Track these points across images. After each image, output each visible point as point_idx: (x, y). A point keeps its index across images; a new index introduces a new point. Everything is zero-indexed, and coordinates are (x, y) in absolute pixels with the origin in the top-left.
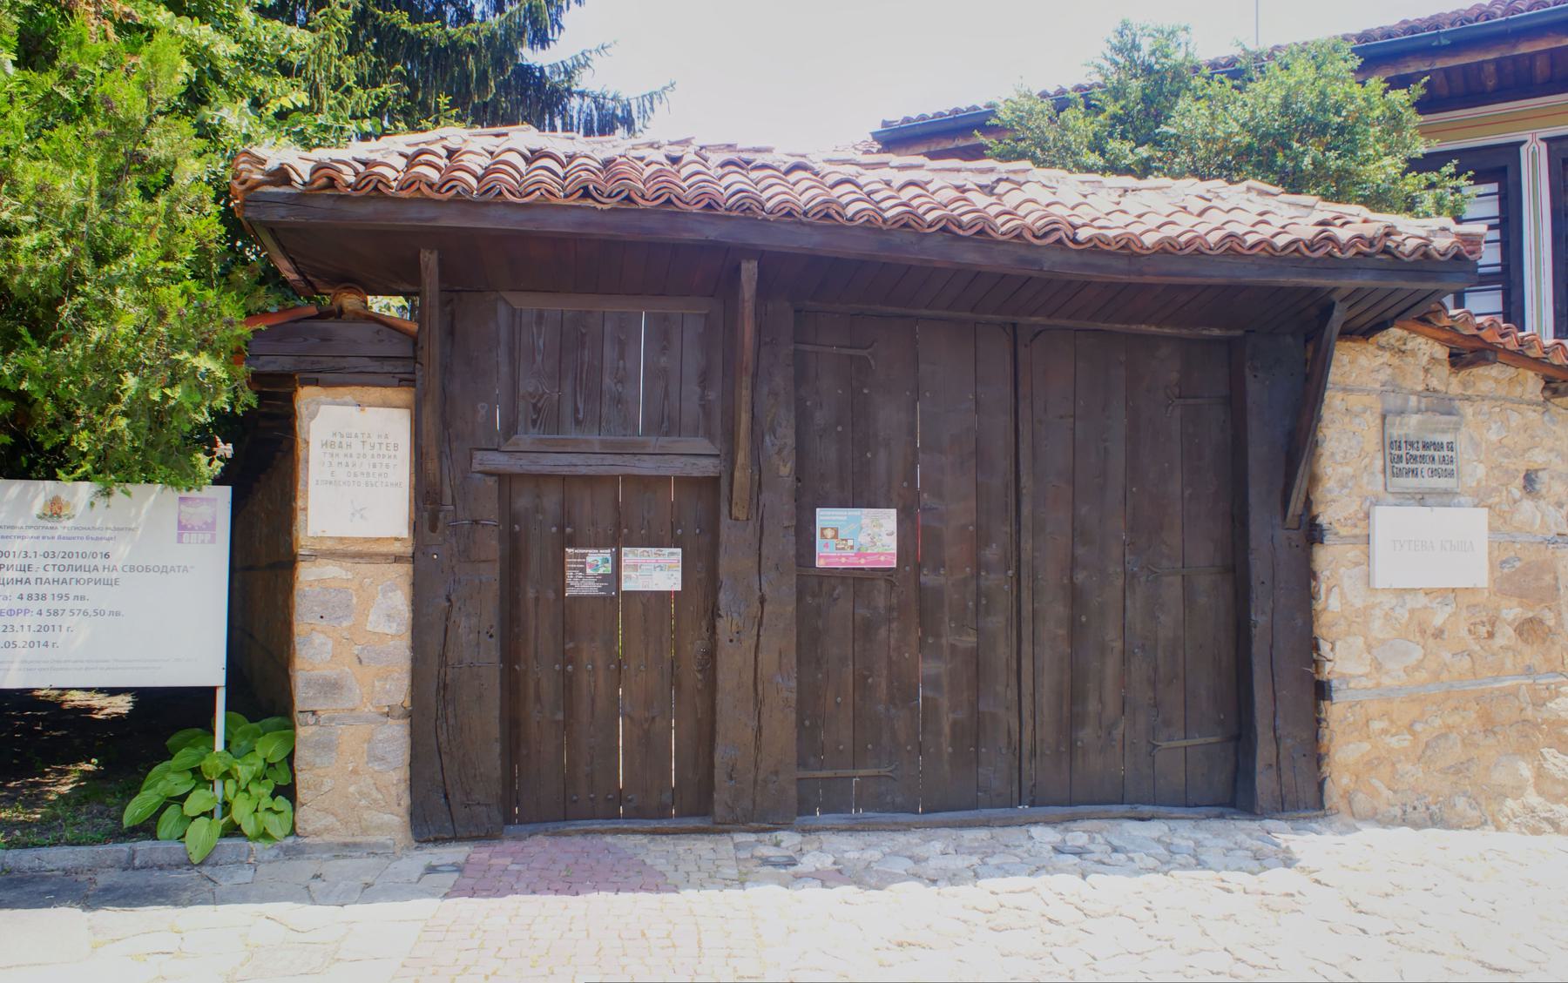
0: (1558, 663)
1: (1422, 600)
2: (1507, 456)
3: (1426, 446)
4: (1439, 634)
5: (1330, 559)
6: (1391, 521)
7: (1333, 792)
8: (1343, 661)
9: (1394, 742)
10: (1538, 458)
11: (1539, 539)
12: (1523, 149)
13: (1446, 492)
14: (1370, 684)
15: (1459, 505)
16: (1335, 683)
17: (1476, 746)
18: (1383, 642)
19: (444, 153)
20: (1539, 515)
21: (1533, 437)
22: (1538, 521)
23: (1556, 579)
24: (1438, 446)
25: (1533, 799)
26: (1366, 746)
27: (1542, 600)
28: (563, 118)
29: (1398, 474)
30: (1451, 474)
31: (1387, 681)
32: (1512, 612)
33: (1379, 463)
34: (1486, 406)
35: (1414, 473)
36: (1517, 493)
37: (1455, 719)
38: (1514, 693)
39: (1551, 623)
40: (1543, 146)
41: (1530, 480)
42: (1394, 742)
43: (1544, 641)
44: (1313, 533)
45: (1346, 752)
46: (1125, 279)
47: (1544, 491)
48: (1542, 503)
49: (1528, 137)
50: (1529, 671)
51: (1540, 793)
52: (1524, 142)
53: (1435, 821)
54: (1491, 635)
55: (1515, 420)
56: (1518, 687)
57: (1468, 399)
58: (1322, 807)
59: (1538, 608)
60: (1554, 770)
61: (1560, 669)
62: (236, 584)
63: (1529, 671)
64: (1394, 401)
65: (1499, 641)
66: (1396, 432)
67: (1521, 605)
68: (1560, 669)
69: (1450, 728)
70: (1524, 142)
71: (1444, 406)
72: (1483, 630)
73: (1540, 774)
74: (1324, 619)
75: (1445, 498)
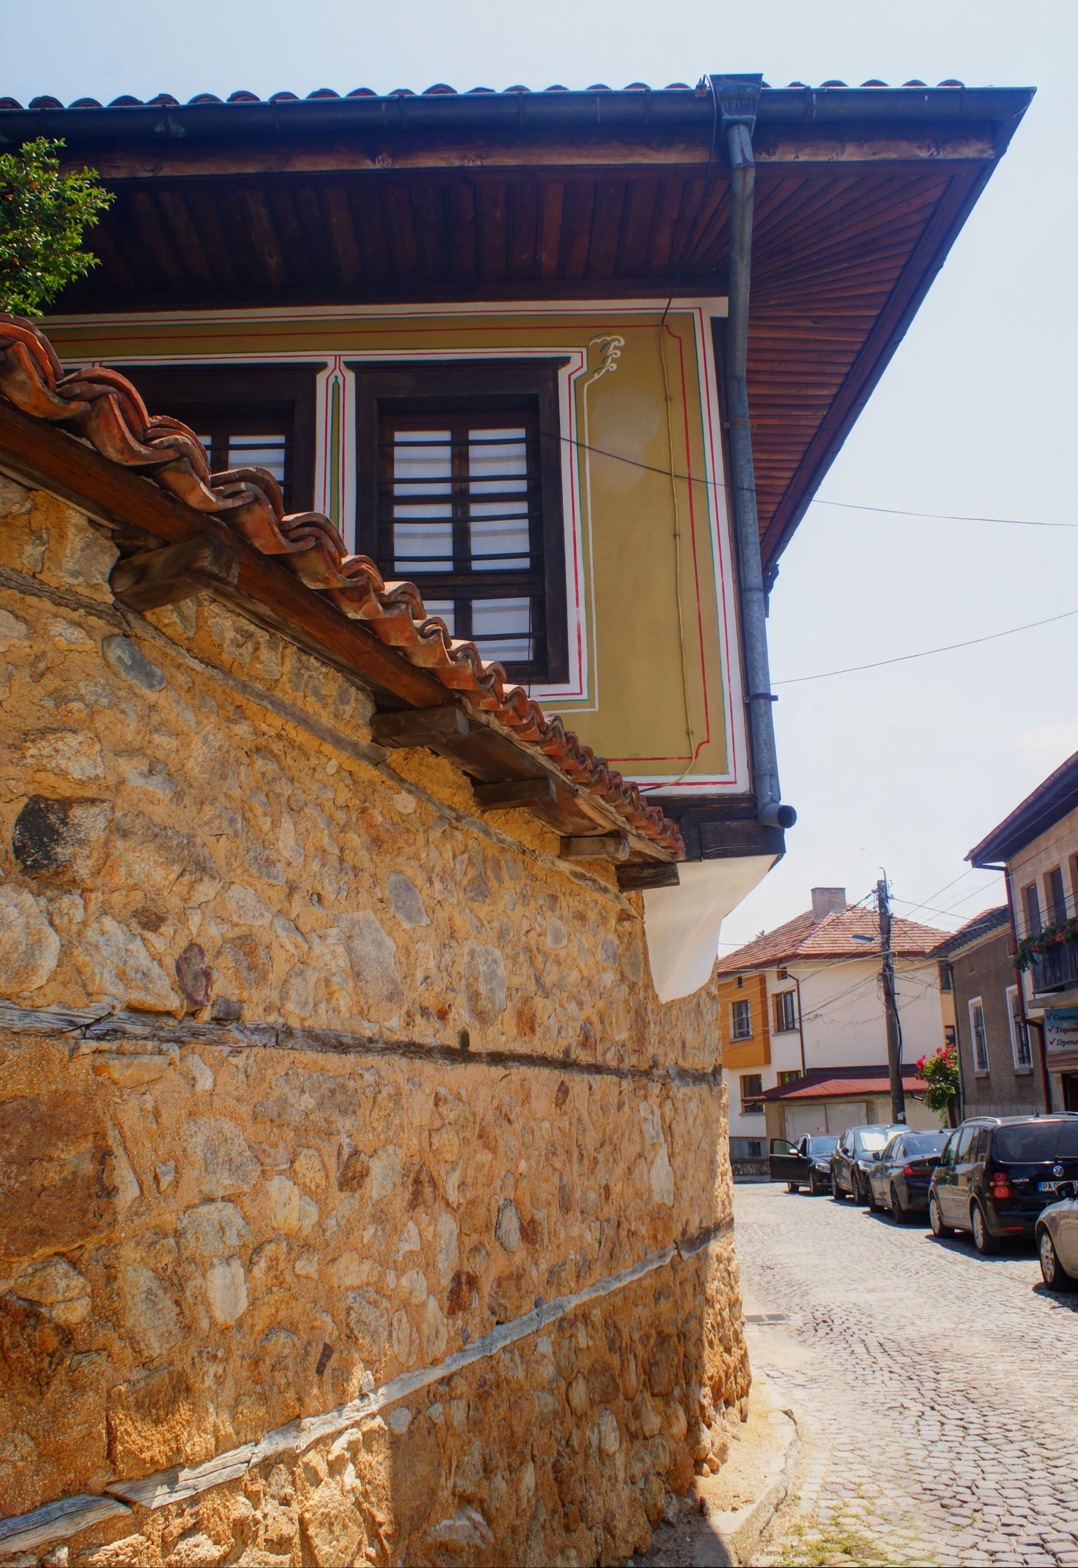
0: (92, 1457)
10: (75, 761)
11: (47, 1020)
12: (321, 378)
19: (886, 1492)
20: (53, 942)
21: (60, 698)
22: (48, 961)
23: (103, 1156)
27: (41, 1235)
28: (687, 1410)
39: (76, 1312)
40: (351, 377)
43: (40, 1383)
46: (73, 505)
47: (83, 868)
48: (71, 905)
52: (323, 366)
59: (24, 1265)
61: (98, 1480)
62: (551, 384)
68: (98, 1480)
70: (323, 366)
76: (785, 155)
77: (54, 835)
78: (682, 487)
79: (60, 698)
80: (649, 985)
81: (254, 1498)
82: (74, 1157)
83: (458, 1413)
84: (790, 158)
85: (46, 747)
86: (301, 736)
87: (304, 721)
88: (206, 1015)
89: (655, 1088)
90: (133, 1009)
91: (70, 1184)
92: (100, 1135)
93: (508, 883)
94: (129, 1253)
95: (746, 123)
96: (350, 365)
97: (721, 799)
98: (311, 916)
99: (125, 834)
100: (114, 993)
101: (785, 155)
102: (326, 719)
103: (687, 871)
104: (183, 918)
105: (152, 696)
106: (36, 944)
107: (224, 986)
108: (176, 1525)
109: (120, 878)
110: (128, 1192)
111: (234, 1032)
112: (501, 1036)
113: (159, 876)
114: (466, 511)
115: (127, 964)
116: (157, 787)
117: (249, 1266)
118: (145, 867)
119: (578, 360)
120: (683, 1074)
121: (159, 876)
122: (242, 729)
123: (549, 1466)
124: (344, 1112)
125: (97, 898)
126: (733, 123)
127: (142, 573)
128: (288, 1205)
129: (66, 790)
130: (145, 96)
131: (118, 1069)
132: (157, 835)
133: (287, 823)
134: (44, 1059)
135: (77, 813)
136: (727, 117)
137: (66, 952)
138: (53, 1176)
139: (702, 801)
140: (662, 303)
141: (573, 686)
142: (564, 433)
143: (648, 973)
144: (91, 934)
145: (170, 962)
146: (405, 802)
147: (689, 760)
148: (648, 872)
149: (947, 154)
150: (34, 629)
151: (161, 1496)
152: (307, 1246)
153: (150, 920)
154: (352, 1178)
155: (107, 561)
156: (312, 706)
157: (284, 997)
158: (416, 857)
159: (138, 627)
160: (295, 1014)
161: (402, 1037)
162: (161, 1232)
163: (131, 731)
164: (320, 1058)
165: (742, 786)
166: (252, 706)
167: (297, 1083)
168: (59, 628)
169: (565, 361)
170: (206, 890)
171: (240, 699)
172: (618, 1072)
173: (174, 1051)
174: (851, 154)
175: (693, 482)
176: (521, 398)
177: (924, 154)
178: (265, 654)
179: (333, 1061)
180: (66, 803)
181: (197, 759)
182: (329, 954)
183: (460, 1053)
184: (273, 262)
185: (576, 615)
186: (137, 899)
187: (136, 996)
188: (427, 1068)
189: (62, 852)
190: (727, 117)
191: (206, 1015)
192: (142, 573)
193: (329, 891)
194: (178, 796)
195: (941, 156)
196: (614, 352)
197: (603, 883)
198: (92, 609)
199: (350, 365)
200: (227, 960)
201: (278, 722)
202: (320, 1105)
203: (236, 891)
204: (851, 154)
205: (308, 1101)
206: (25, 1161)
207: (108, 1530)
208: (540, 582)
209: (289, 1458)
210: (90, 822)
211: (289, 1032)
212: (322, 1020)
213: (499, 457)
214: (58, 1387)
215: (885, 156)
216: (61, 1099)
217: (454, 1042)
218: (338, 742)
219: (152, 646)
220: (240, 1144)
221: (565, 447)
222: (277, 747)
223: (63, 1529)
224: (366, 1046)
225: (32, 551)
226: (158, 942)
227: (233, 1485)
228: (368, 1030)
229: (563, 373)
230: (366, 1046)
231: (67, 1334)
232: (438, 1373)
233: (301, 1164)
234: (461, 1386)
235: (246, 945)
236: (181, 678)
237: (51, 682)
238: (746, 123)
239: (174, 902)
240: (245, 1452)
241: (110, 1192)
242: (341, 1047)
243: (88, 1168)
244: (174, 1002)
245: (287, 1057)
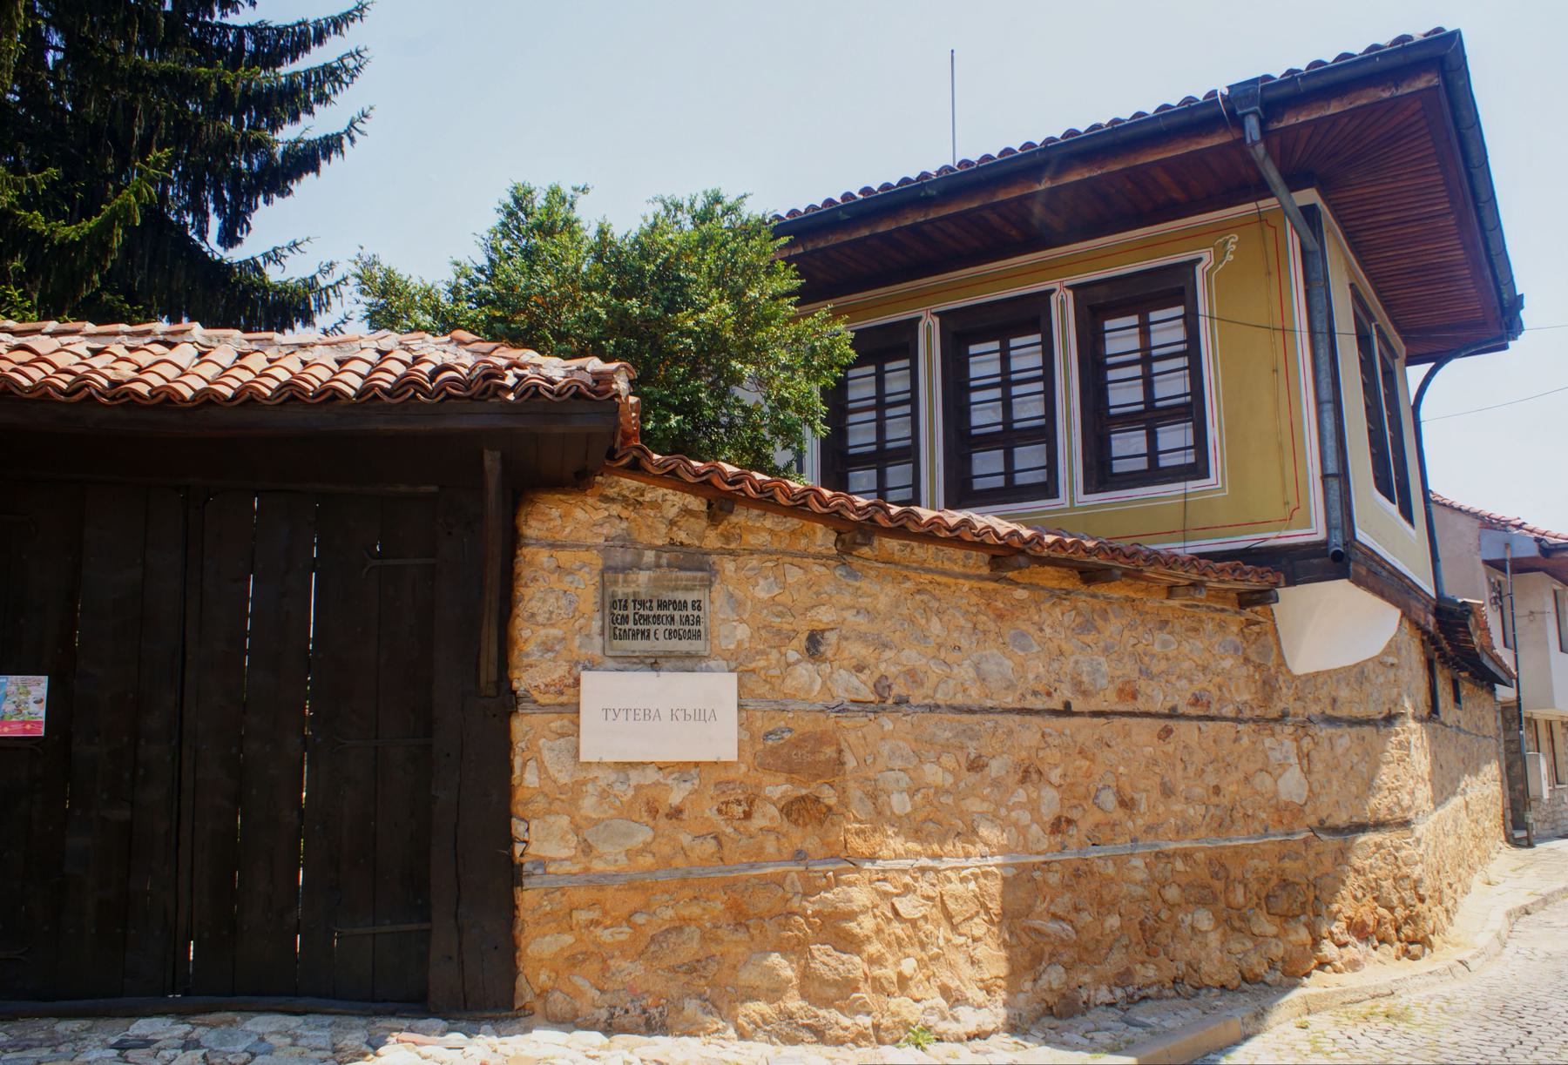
1: (652, 776)
2: (781, 615)
3: (663, 605)
4: (676, 813)
5: (529, 730)
6: (602, 691)
7: (526, 992)
8: (543, 840)
9: (605, 935)
10: (825, 616)
11: (818, 707)
12: (1053, 298)
13: (689, 656)
14: (576, 869)
15: (709, 670)
16: (527, 867)
17: (718, 940)
18: (596, 823)
20: (819, 681)
21: (818, 594)
22: (817, 687)
23: (840, 751)
24: (683, 605)
25: (794, 1003)
26: (568, 939)
27: (819, 776)
29: (624, 635)
30: (698, 635)
31: (598, 866)
32: (778, 789)
33: (596, 625)
34: (754, 562)
35: (645, 635)
36: (793, 656)
37: (695, 910)
38: (779, 881)
39: (832, 801)
40: (1070, 294)
41: (814, 642)
42: (605, 935)
43: (821, 823)
44: (508, 702)
45: (540, 947)
47: (829, 654)
48: (826, 667)
49: (1057, 286)
50: (799, 856)
51: (803, 997)
52: (1053, 290)
53: (651, 1027)
54: (748, 815)
55: (794, 575)
56: (785, 875)
57: (732, 553)
58: (510, 1006)
59: (814, 785)
60: (822, 969)
61: (843, 855)
63: (799, 856)
64: (620, 557)
65: (758, 822)
66: (620, 591)
67: (790, 781)
69: (687, 921)
70: (1053, 290)
71: (694, 561)
72: (738, 811)
73: (806, 976)
74: (519, 795)
75: (689, 662)
76: (1290, 120)
77: (819, 642)
78: (1279, 334)
79: (818, 594)
80: (1282, 662)
81: (916, 879)
82: (830, 751)
83: (1054, 879)
84: (1293, 121)
85: (813, 612)
86: (943, 579)
87: (944, 573)
88: (890, 701)
89: (1289, 730)
90: (854, 701)
91: (828, 761)
92: (838, 744)
93: (1113, 620)
94: (851, 784)
95: (1255, 113)
96: (1069, 287)
97: (1307, 545)
98: (952, 657)
99: (847, 639)
100: (842, 695)
101: (1290, 120)
102: (957, 569)
103: (1284, 593)
104: (877, 666)
105: (857, 584)
106: (812, 682)
107: (898, 689)
108: (875, 877)
109: (846, 654)
110: (851, 763)
111: (904, 707)
112: (1109, 701)
113: (863, 652)
114: (1150, 368)
115: (850, 686)
116: (861, 619)
117: (912, 796)
118: (857, 650)
119: (1207, 256)
120: (1332, 721)
121: (863, 652)
122: (908, 585)
123: (1136, 922)
124: (971, 739)
125: (836, 664)
126: (1244, 115)
127: (844, 542)
128: (934, 774)
129: (822, 627)
130: (914, 175)
131: (844, 722)
132: (862, 637)
133: (935, 620)
134: (817, 720)
135: (827, 634)
136: (1239, 112)
137: (824, 683)
138: (822, 757)
139: (1295, 547)
140: (1252, 205)
141: (1212, 480)
142: (1201, 311)
143: (1280, 655)
144: (835, 676)
145: (871, 684)
146: (1021, 594)
147: (1288, 521)
148: (1255, 597)
149: (1405, 90)
150: (805, 570)
151: (868, 865)
152: (947, 792)
153: (860, 669)
154: (976, 765)
155: (833, 538)
156: (948, 565)
157: (935, 692)
158: (1030, 619)
159: (849, 559)
160: (940, 698)
161: (1018, 706)
162: (867, 779)
163: (847, 599)
164: (958, 717)
165: (1321, 535)
166: (911, 574)
167: (943, 728)
168: (816, 568)
169: (1199, 260)
170: (888, 654)
171: (905, 573)
172: (1237, 720)
173: (872, 716)
174: (1334, 108)
175: (1286, 331)
176: (1171, 287)
177: (1386, 95)
178: (916, 551)
179: (965, 717)
180: (823, 631)
181: (883, 602)
182: (965, 672)
183: (1067, 711)
184: (1013, 233)
185: (1213, 433)
186: (854, 662)
187: (855, 697)
188: (1036, 720)
189: (822, 649)
190: (1239, 112)
191: (890, 701)
192: (844, 542)
193: (964, 643)
194: (872, 620)
195: (1399, 92)
196: (1231, 247)
197: (1218, 606)
198: (828, 558)
199: (1069, 287)
200: (901, 680)
201: (929, 577)
202: (957, 735)
203: (906, 652)
204: (1334, 108)
205: (948, 734)
206: (813, 753)
207: (847, 871)
208: (1191, 411)
209: (937, 871)
210: (832, 637)
211: (938, 707)
212: (959, 700)
213: (1167, 330)
214: (827, 824)
215: (1358, 103)
216: (824, 733)
217: (1060, 707)
218: (967, 577)
219: (857, 563)
220: (908, 750)
221: (1201, 320)
222: (929, 587)
223: (830, 867)
224: (991, 710)
225: (804, 542)
226: (862, 677)
227: (904, 871)
228: (989, 703)
229: (1199, 268)
230: (991, 710)
231: (829, 808)
232: (1041, 858)
233: (944, 759)
234: (1056, 866)
235: (912, 674)
236: (872, 573)
237: (815, 588)
238: (1255, 113)
239: (872, 661)
240: (910, 862)
241: (843, 764)
242: (971, 711)
243: (835, 755)
244: (872, 698)
245: (936, 716)
